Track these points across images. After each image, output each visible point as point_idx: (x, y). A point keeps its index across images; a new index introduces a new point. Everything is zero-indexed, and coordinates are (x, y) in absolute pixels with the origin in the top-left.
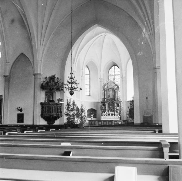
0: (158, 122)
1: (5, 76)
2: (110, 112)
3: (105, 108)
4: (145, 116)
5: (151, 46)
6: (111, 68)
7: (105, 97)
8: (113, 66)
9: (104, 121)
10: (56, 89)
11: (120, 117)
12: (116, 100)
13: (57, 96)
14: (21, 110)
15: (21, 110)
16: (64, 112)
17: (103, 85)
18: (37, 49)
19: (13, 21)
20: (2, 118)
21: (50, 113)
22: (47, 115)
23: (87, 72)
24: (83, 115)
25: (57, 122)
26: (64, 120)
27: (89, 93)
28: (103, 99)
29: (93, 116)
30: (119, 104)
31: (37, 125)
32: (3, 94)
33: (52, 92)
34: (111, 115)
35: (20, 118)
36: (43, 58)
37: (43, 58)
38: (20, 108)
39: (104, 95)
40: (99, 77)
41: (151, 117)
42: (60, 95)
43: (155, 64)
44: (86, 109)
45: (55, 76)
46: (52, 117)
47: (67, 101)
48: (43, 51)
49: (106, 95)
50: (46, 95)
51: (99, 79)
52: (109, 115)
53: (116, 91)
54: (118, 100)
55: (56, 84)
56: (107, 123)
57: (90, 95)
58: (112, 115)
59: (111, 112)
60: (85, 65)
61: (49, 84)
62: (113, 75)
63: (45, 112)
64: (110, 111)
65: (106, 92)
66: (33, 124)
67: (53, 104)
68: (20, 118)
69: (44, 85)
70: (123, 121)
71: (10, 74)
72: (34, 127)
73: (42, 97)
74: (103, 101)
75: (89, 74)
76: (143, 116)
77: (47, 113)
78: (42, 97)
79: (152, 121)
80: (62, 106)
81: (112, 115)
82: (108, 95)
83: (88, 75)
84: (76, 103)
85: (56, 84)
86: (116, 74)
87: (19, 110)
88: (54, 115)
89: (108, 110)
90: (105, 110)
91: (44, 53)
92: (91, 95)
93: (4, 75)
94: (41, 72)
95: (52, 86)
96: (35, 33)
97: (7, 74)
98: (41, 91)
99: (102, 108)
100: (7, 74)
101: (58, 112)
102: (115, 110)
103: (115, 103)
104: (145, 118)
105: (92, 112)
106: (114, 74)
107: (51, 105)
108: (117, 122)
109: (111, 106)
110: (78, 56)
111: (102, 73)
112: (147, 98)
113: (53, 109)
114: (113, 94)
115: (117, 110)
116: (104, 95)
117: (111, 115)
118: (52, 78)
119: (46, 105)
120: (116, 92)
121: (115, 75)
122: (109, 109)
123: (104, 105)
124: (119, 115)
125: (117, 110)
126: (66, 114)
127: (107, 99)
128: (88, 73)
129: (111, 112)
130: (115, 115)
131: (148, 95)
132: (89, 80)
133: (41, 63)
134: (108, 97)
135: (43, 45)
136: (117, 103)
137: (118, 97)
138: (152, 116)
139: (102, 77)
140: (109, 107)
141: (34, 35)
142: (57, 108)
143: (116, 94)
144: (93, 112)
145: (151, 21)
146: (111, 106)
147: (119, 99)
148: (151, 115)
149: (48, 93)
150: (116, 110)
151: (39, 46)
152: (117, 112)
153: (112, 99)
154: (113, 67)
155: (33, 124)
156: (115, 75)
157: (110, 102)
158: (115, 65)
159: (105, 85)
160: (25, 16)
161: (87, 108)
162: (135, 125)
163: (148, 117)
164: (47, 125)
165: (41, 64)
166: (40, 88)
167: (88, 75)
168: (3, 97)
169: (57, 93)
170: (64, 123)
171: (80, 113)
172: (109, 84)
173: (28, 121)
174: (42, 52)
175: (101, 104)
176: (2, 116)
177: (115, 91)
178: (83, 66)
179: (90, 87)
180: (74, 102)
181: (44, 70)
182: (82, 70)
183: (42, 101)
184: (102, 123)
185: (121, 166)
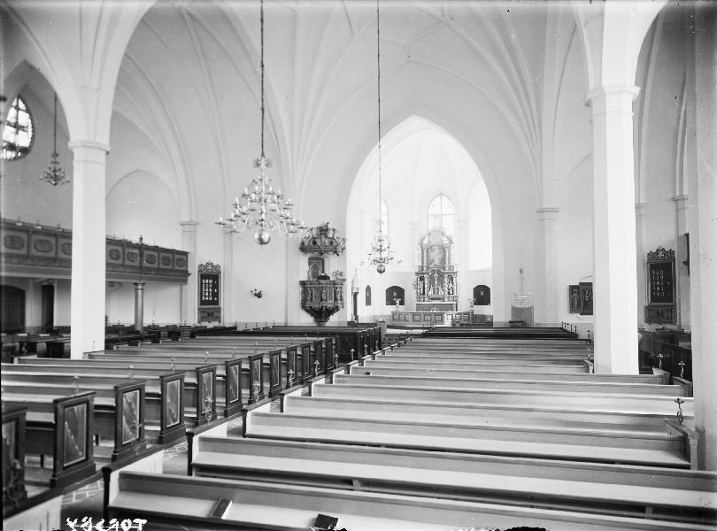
7: (423, 262)
13: (332, 266)
17: (417, 242)
22: (316, 306)
33: (322, 257)
38: (257, 292)
39: (423, 259)
41: (530, 310)
45: (329, 226)
46: (326, 309)
50: (310, 263)
53: (447, 250)
55: (331, 243)
61: (319, 243)
63: (311, 299)
66: (286, 323)
69: (306, 244)
78: (303, 270)
85: (331, 243)
87: (255, 295)
88: (329, 306)
95: (320, 246)
96: (287, 139)
101: (336, 299)
109: (436, 282)
113: (326, 293)
114: (441, 257)
116: (423, 259)
118: (323, 230)
123: (422, 279)
127: (428, 267)
145: (535, 111)
146: (436, 282)
148: (530, 305)
154: (438, 199)
155: (286, 323)
158: (441, 194)
159: (423, 239)
166: (298, 250)
176: (222, 307)
177: (444, 250)
183: (305, 278)
185: (68, 130)
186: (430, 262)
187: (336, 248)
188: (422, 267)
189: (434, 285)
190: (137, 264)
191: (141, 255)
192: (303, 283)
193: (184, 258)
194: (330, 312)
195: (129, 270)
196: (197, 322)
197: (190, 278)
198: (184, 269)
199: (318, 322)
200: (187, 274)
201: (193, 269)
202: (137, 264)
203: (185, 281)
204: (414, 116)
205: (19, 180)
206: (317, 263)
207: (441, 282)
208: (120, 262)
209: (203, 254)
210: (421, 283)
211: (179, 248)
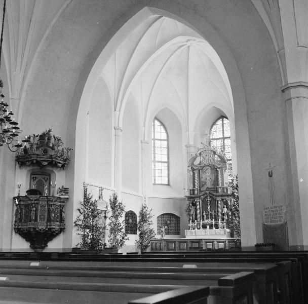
0: (302, 241)
2: (206, 221)
3: (196, 210)
4: (269, 224)
5: (271, 32)
6: (214, 123)
7: (194, 186)
8: (219, 119)
9: (193, 241)
10: (60, 165)
11: (228, 230)
12: (220, 190)
13: (59, 180)
16: (75, 219)
18: (8, 73)
21: (30, 221)
23: (160, 132)
24: (146, 227)
25: (55, 245)
27: (167, 179)
28: (190, 190)
29: (166, 230)
30: (227, 201)
34: (208, 227)
36: (24, 94)
37: (24, 94)
39: (194, 182)
40: (184, 144)
41: (283, 227)
42: (66, 173)
43: (285, 76)
44: (152, 213)
45: (52, 134)
48: (24, 78)
49: (196, 182)
51: (184, 148)
52: (204, 227)
54: (225, 191)
56: (175, 246)
57: (169, 185)
58: (211, 227)
59: (209, 221)
60: (150, 115)
64: (207, 218)
65: (196, 175)
66: (11, 249)
70: (229, 242)
74: (191, 194)
75: (166, 138)
76: (264, 225)
78: (20, 182)
79: (285, 238)
80: (68, 205)
81: (211, 227)
82: (202, 180)
83: (164, 140)
84: (119, 200)
86: (225, 136)
88: (40, 227)
89: (203, 216)
90: (196, 215)
92: (171, 183)
98: (18, 170)
99: (190, 210)
102: (218, 216)
103: (219, 199)
104: (268, 231)
105: (169, 222)
106: (222, 137)
107: (33, 202)
108: (213, 245)
109: (209, 207)
111: (192, 133)
112: (270, 175)
114: (213, 178)
115: (223, 215)
116: (194, 182)
117: (208, 227)
118: (44, 138)
120: (219, 173)
121: (224, 138)
122: (205, 213)
123: (194, 205)
124: (228, 228)
125: (223, 215)
126: (80, 223)
128: (164, 136)
129: (209, 221)
130: (217, 227)
131: (272, 166)
132: (166, 153)
133: (19, 104)
134: (203, 185)
136: (223, 200)
137: (225, 185)
138: (286, 223)
139: (191, 143)
140: (204, 207)
142: (49, 210)
143: (220, 179)
144: (172, 222)
146: (209, 207)
147: (227, 189)
149: (37, 176)
150: (220, 214)
152: (223, 219)
153: (211, 188)
154: (220, 122)
156: (224, 138)
157: (206, 197)
159: (195, 159)
161: (155, 212)
163: (275, 228)
164: (31, 251)
167: (164, 140)
170: (74, 246)
172: (203, 155)
174: (21, 81)
175: (187, 202)
177: (217, 171)
178: (145, 117)
179: (168, 167)
182: (144, 128)
184: (177, 246)
186: (202, 184)
187: (65, 163)
188: (193, 190)
189: (206, 210)
194: (51, 235)
204: (146, 9)
207: (215, 207)
210: (193, 209)
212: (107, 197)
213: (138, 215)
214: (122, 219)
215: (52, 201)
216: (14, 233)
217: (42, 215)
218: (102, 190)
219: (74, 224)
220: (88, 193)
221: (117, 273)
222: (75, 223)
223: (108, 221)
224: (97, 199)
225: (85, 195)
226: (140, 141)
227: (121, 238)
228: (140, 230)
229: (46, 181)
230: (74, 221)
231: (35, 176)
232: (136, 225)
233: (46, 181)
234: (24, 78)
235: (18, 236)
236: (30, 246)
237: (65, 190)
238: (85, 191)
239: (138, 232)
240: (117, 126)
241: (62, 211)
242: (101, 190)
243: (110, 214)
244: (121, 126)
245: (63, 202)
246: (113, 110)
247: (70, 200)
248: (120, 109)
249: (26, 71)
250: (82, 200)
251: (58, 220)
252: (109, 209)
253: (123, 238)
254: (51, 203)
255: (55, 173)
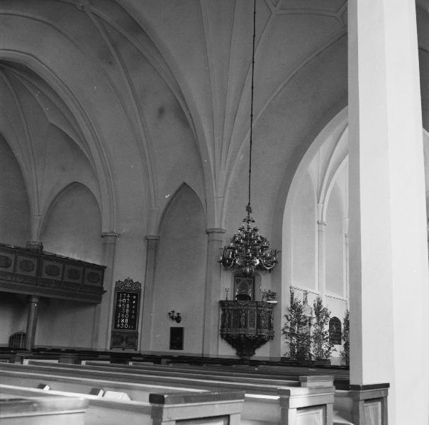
1: (147, 239)
14: (178, 319)
15: (178, 319)
16: (283, 326)
19: (161, 111)
20: (137, 338)
22: (233, 332)
26: (283, 347)
31: (211, 357)
32: (141, 281)
35: (177, 337)
36: (228, 191)
37: (228, 191)
38: (175, 315)
42: (272, 279)
47: (292, 298)
48: (228, 175)
62: (111, 244)
63: (229, 326)
67: (247, 305)
68: (177, 337)
71: (159, 232)
72: (200, 362)
73: (225, 287)
77: (234, 327)
78: (225, 287)
84: (324, 305)
87: (172, 318)
91: (230, 180)
93: (145, 235)
94: (221, 225)
97: (35, 240)
100: (153, 233)
110: (330, 179)
113: (246, 317)
119: (230, 308)
126: (288, 331)
133: (223, 202)
135: (228, 159)
141: (203, 134)
142: (258, 316)
151: (217, 162)
160: (180, 92)
162: (332, 377)
165: (223, 206)
168: (142, 288)
169: (263, 277)
170: (282, 356)
171: (342, 331)
173: (191, 347)
176: (139, 332)
180: (320, 303)
181: (226, 221)
187: (273, 264)
190: (33, 274)
191: (40, 264)
192: (222, 304)
193: (100, 273)
194: (260, 342)
195: (18, 280)
196: (109, 348)
197: (104, 297)
198: (98, 285)
199: (240, 356)
200: (101, 291)
201: (110, 287)
202: (33, 274)
203: (99, 300)
205: (269, 255)
206: (245, 279)
208: (10, 270)
209: (127, 267)
211: (98, 263)
212: (311, 302)
213: (342, 321)
214: (326, 328)
215: (261, 307)
216: (220, 338)
217: (252, 320)
218: (306, 294)
219: (282, 332)
220: (295, 297)
221: (269, 386)
222: (283, 330)
223: (313, 329)
224: (302, 303)
225: (292, 302)
226: (344, 236)
227: (327, 349)
228: (344, 339)
229: (250, 284)
230: (282, 328)
231: (239, 278)
232: (341, 334)
233: (250, 284)
234: (228, 175)
235: (224, 341)
236: (237, 354)
237: (272, 295)
238: (292, 294)
239: (343, 342)
240: (320, 220)
241: (270, 317)
242: (306, 293)
243: (314, 321)
244: (324, 220)
245: (272, 308)
246: (316, 202)
247: (277, 306)
248: (324, 200)
249: (230, 169)
250: (289, 306)
251: (267, 326)
252: (314, 315)
253: (330, 349)
254: (261, 309)
255: (259, 275)
